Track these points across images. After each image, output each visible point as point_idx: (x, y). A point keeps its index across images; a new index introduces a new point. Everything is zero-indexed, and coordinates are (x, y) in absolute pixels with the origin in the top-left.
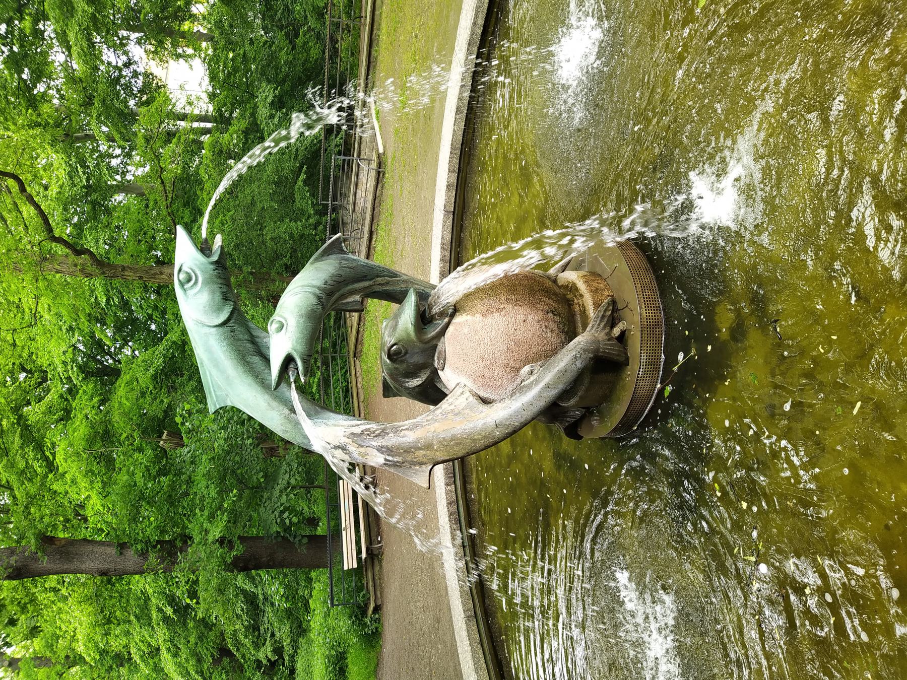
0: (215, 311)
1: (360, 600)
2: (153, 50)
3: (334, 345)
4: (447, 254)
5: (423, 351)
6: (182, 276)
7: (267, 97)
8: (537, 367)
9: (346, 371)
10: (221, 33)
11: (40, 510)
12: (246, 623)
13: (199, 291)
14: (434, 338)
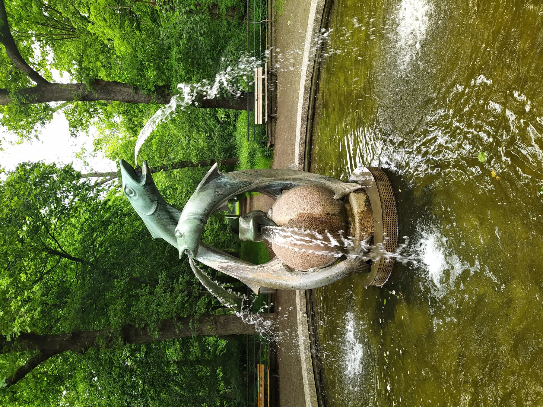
0: (147, 208)
4: (320, 16)
11: (88, 58)
13: (137, 199)
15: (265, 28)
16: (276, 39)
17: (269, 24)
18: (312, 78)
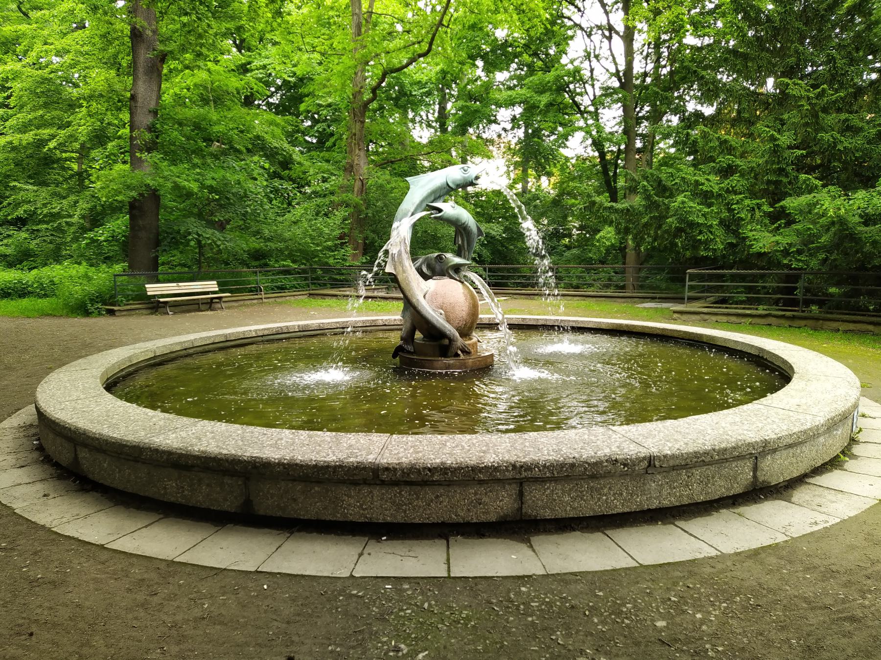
1: (119, 298)
2: (512, 147)
3: (317, 279)
5: (442, 270)
6: (466, 168)
7: (494, 230)
8: (443, 316)
9: (297, 288)
10: (529, 199)
12: (39, 211)
14: (449, 274)
15: (252, 291)
16: (245, 305)
17: (261, 297)
18: (385, 325)
